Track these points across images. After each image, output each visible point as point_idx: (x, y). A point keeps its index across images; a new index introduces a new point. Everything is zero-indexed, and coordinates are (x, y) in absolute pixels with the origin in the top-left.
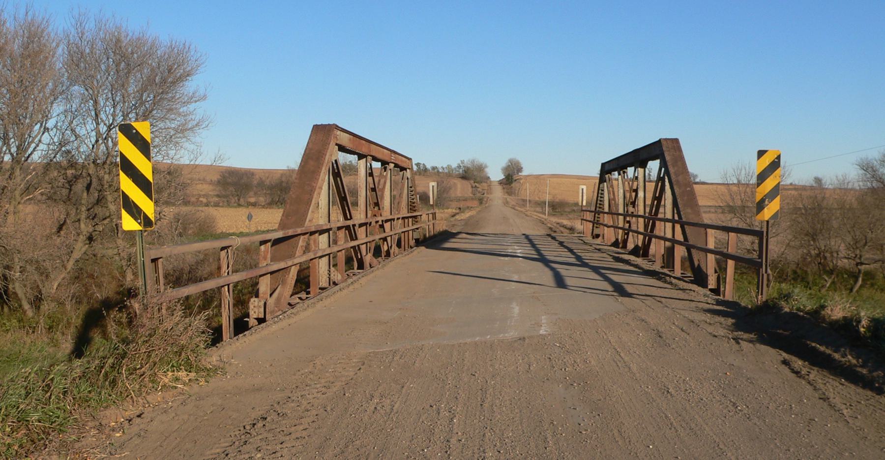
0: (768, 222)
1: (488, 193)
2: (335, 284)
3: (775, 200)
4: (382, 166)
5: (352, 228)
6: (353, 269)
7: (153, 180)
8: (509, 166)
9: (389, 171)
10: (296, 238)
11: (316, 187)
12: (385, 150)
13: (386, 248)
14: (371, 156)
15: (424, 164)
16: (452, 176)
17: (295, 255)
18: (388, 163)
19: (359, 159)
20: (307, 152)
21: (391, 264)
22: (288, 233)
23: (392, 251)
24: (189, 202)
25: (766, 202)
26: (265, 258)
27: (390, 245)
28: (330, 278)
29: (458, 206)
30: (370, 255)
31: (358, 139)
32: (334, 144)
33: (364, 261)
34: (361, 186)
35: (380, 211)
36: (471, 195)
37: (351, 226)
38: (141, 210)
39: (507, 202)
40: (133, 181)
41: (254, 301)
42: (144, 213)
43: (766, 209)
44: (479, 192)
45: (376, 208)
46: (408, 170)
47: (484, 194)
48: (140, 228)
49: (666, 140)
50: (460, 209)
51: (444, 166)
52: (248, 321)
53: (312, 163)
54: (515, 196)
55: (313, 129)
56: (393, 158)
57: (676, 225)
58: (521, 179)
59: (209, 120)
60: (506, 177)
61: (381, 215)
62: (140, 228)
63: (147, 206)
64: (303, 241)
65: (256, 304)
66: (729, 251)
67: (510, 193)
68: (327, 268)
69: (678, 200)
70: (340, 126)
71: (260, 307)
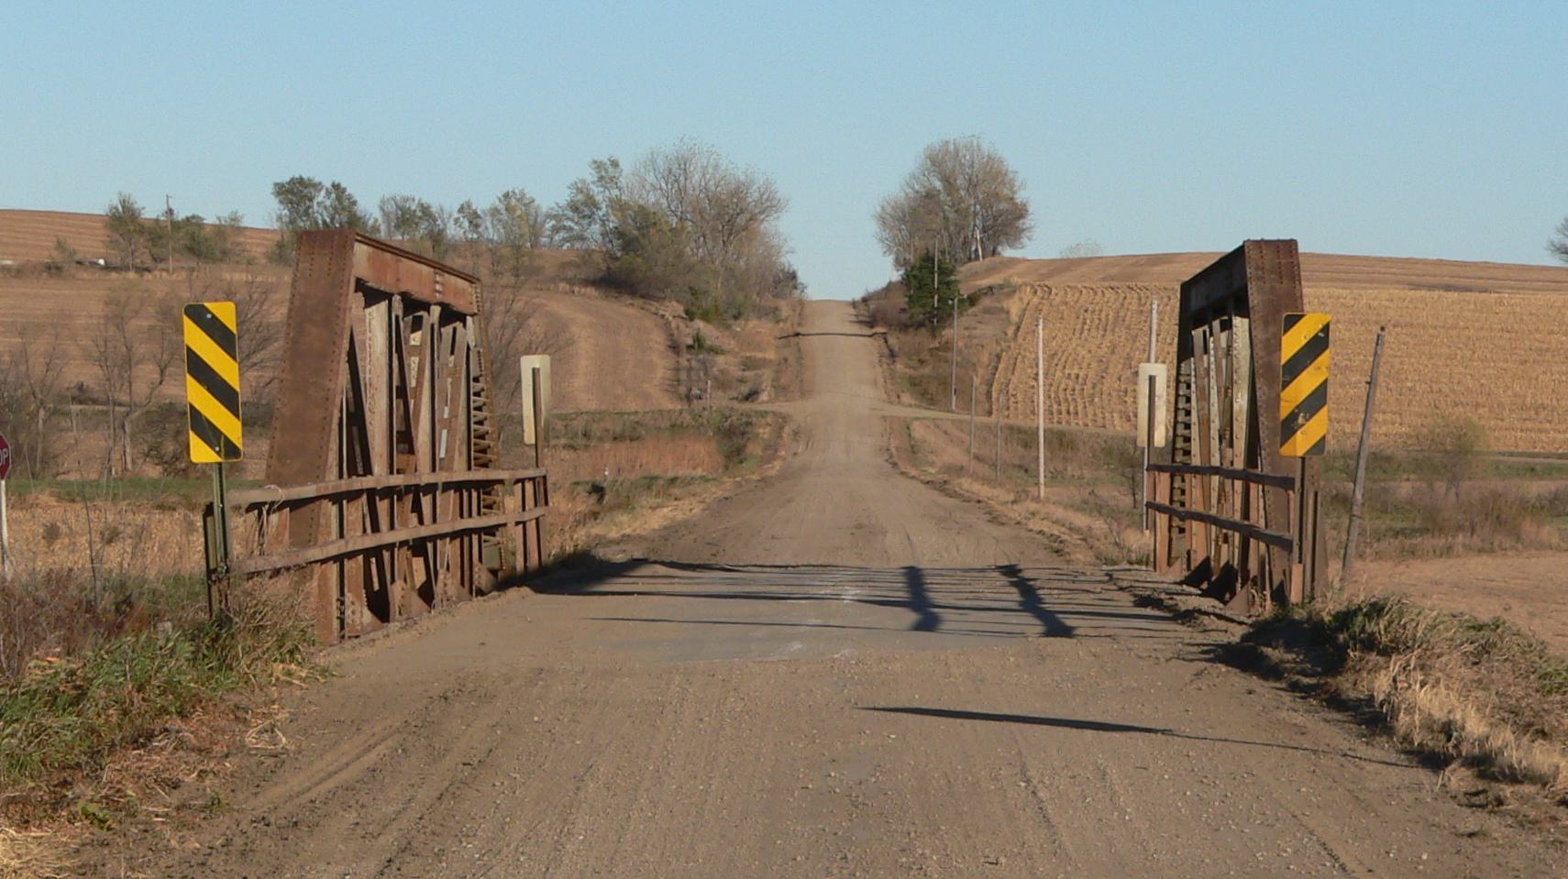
0: (1303, 459)
1: (781, 390)
3: (1316, 417)
7: (241, 388)
8: (930, 196)
10: (312, 506)
15: (336, 187)
16: (534, 271)
19: (368, 304)
25: (1300, 420)
29: (586, 475)
34: (374, 382)
36: (668, 404)
38: (221, 433)
39: (913, 450)
40: (208, 390)
42: (225, 437)
43: (1299, 433)
44: (722, 385)
46: (469, 319)
47: (751, 396)
48: (217, 459)
49: (1261, 244)
50: (598, 490)
51: (483, 203)
54: (967, 405)
57: (1252, 485)
58: (1008, 290)
60: (906, 281)
62: (217, 459)
63: (230, 426)
66: (1158, 500)
67: (928, 391)
69: (1261, 419)
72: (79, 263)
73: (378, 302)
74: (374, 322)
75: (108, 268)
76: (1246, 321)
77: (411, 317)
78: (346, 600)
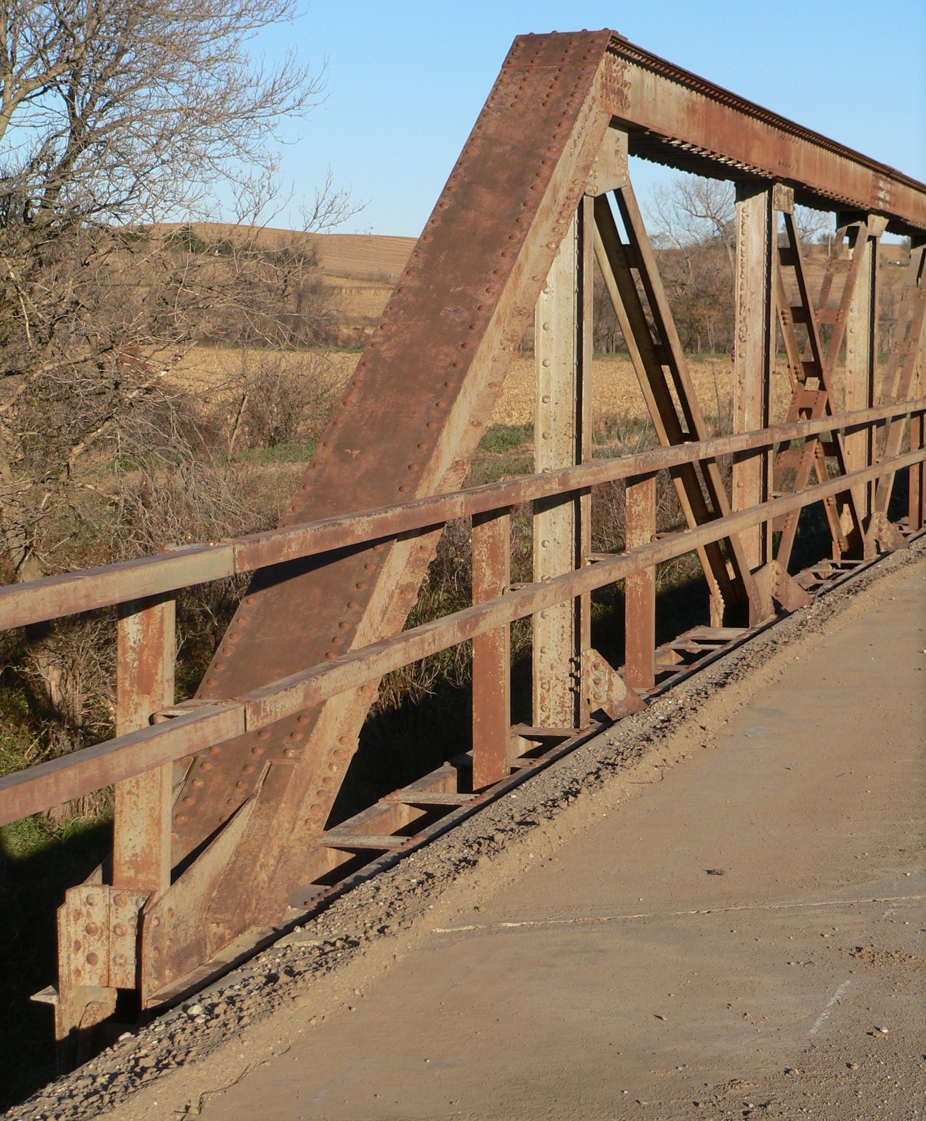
2: (604, 720)
4: (840, 224)
5: (700, 476)
6: (705, 620)
9: (868, 245)
11: (493, 307)
12: (852, 165)
13: (846, 525)
14: (788, 182)
17: (348, 643)
18: (863, 215)
19: (742, 195)
20: (475, 152)
21: (861, 603)
22: (277, 548)
23: (869, 539)
24: (336, 338)
26: (145, 684)
27: (861, 515)
28: (577, 695)
30: (775, 569)
31: (728, 111)
32: (605, 119)
33: (750, 592)
34: (747, 300)
35: (824, 396)
37: (698, 469)
41: (89, 902)
45: (813, 383)
52: (51, 1008)
53: (487, 198)
55: (512, 52)
56: (885, 191)
59: (306, 83)
61: (829, 412)
64: (413, 563)
65: (98, 916)
68: (568, 649)
70: (632, 40)
71: (117, 931)
72: (890, 263)
73: (757, 194)
74: (748, 221)
75: (901, 265)
76: (715, 464)
77: (846, 228)
78: (583, 661)
